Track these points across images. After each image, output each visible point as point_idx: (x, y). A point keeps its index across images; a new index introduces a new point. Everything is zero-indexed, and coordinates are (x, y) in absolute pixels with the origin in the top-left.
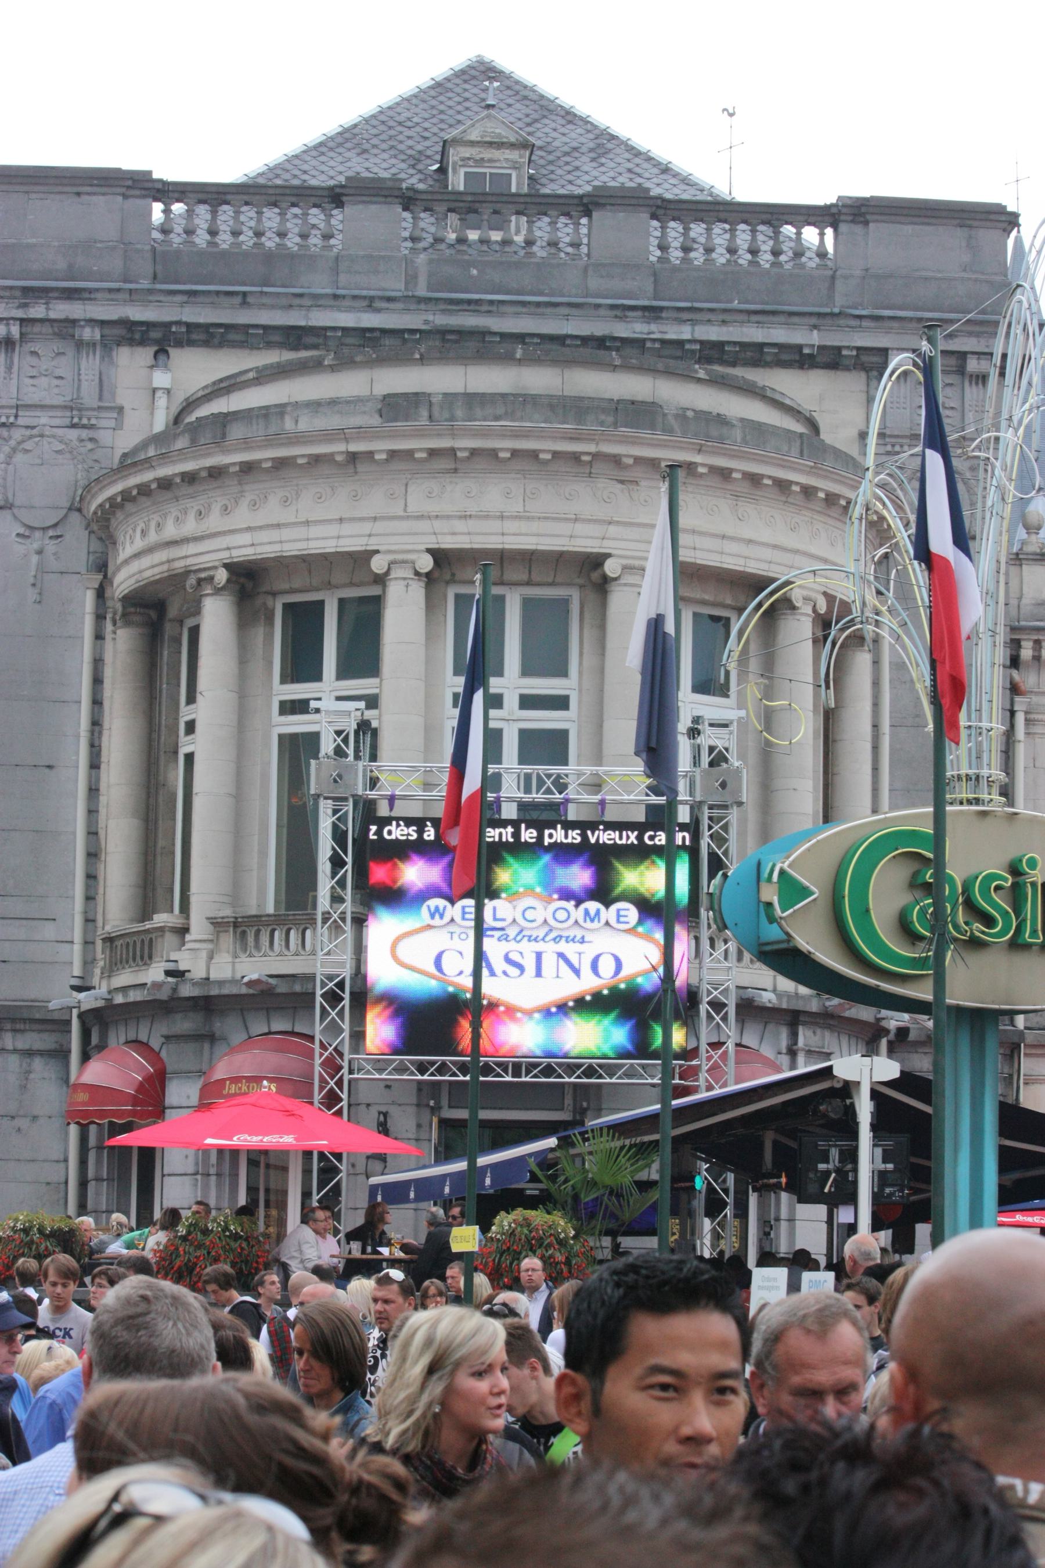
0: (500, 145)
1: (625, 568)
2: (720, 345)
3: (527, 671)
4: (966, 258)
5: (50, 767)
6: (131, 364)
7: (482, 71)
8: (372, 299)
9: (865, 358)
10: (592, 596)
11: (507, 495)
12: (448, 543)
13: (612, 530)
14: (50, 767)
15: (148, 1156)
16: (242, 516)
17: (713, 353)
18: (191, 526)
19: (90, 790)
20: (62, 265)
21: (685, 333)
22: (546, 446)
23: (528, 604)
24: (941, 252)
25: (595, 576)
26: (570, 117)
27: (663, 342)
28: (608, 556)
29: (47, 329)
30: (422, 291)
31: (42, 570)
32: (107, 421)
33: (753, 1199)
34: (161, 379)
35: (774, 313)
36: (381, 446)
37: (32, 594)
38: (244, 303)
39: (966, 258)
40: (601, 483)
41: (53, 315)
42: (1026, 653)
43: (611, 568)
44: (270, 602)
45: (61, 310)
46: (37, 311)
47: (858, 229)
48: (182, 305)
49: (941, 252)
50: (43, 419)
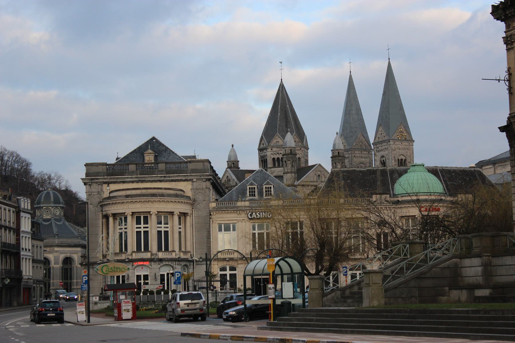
3: (144, 224)
5: (233, 146)
6: (105, 186)
14: (233, 146)
16: (112, 208)
18: (108, 209)
19: (210, 338)
21: (169, 179)
23: (144, 217)
26: (163, 145)
31: (96, 211)
32: (102, 193)
33: (166, 289)
34: (108, 188)
36: (125, 201)
42: (212, 214)
50: (95, 193)
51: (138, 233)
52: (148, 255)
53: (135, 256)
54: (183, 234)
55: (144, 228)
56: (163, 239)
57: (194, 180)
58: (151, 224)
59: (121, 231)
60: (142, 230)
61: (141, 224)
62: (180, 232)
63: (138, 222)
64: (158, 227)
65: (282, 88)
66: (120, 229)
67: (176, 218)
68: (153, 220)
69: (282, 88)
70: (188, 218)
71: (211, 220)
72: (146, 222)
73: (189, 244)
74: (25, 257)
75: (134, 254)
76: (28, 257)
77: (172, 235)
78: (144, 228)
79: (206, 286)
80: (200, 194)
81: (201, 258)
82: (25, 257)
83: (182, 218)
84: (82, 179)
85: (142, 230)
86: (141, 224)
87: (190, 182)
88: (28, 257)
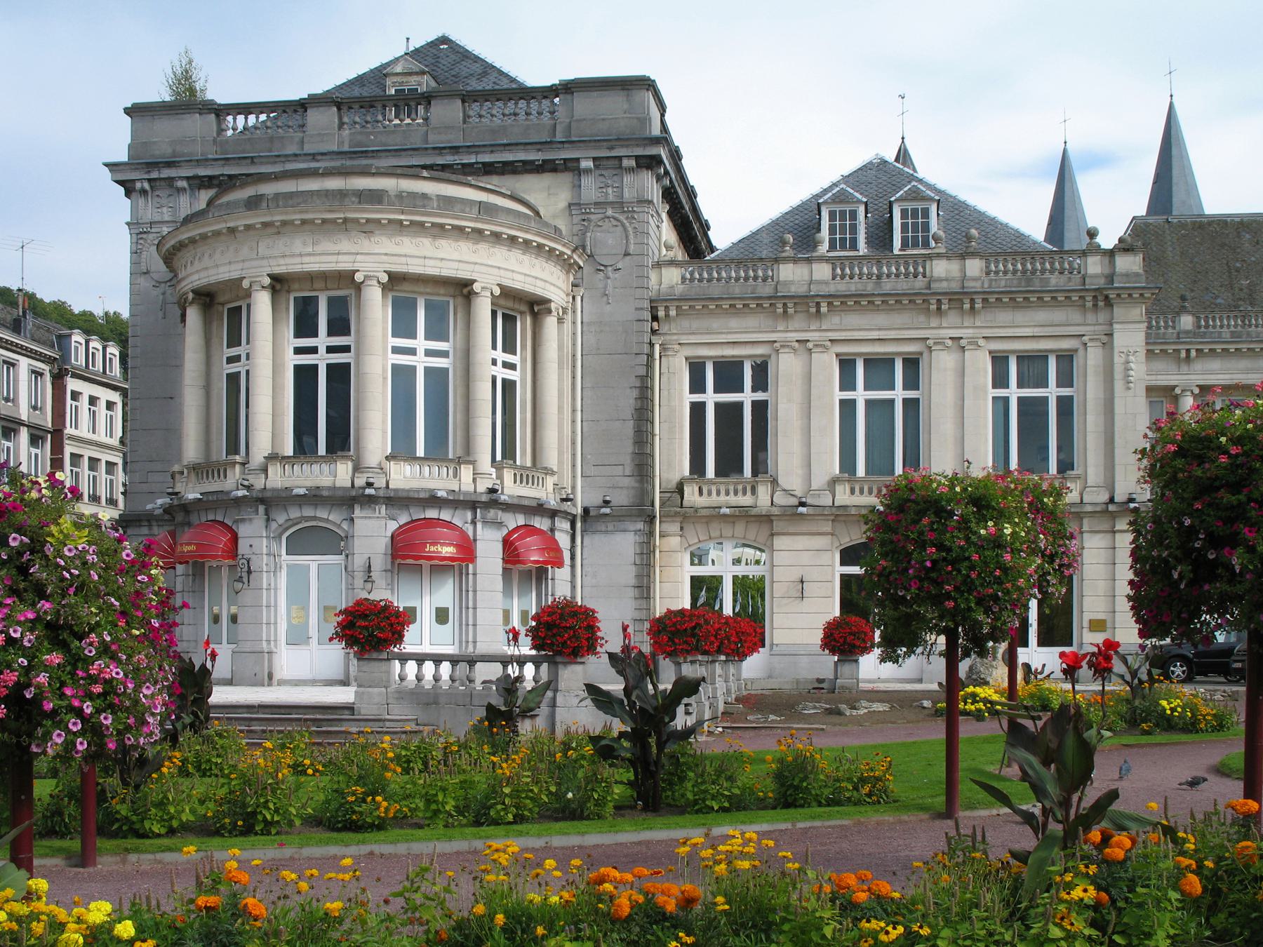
0: (410, 74)
1: (365, 277)
2: (491, 164)
4: (626, 106)
7: (444, 40)
8: (314, 155)
9: (569, 165)
10: (460, 300)
11: (304, 244)
12: (277, 270)
13: (359, 258)
15: (1071, 577)
17: (467, 169)
20: (169, 151)
21: (472, 159)
22: (318, 216)
24: (612, 107)
25: (465, 291)
26: (477, 59)
27: (463, 165)
28: (475, 281)
29: (163, 183)
30: (346, 148)
35: (517, 144)
37: (161, 314)
38: (253, 162)
39: (626, 106)
40: (354, 233)
41: (162, 176)
42: (661, 313)
43: (359, 277)
44: (220, 308)
45: (166, 173)
46: (154, 175)
47: (569, 97)
48: (223, 166)
49: (612, 107)
51: (305, 376)
52: (341, 474)
53: (277, 478)
54: (523, 396)
55: (330, 350)
56: (436, 414)
57: (585, 164)
58: (358, 331)
59: (233, 368)
60: (322, 361)
61: (413, 335)
62: (509, 386)
63: (305, 326)
64: (346, 349)
65: (106, 165)
66: (231, 360)
67: (483, 308)
68: (376, 311)
69: (106, 165)
70: (550, 323)
71: (657, 341)
72: (339, 325)
73: (551, 437)
74: (88, 453)
75: (275, 471)
76: (105, 457)
77: (460, 391)
78: (330, 350)
79: (584, 200)
80: (607, 225)
81: (606, 503)
82: (88, 453)
83: (523, 326)
84: (112, 166)
85: (322, 361)
86: (413, 335)
87: (565, 179)
88: (105, 457)
